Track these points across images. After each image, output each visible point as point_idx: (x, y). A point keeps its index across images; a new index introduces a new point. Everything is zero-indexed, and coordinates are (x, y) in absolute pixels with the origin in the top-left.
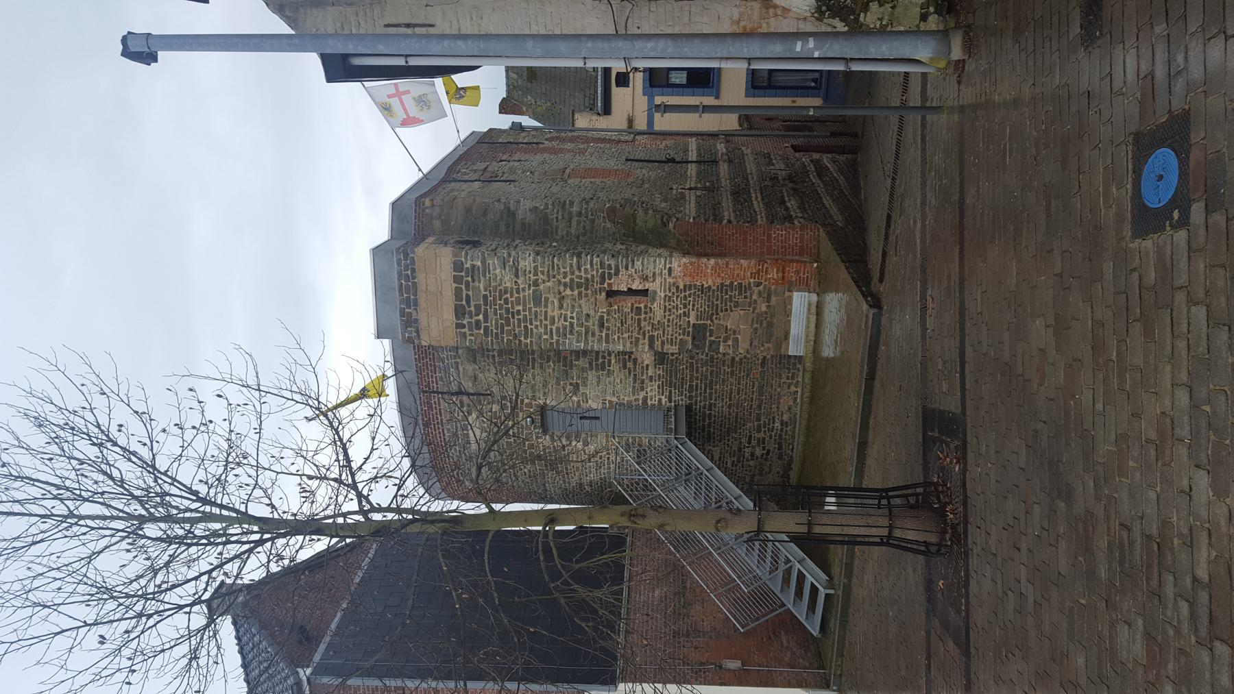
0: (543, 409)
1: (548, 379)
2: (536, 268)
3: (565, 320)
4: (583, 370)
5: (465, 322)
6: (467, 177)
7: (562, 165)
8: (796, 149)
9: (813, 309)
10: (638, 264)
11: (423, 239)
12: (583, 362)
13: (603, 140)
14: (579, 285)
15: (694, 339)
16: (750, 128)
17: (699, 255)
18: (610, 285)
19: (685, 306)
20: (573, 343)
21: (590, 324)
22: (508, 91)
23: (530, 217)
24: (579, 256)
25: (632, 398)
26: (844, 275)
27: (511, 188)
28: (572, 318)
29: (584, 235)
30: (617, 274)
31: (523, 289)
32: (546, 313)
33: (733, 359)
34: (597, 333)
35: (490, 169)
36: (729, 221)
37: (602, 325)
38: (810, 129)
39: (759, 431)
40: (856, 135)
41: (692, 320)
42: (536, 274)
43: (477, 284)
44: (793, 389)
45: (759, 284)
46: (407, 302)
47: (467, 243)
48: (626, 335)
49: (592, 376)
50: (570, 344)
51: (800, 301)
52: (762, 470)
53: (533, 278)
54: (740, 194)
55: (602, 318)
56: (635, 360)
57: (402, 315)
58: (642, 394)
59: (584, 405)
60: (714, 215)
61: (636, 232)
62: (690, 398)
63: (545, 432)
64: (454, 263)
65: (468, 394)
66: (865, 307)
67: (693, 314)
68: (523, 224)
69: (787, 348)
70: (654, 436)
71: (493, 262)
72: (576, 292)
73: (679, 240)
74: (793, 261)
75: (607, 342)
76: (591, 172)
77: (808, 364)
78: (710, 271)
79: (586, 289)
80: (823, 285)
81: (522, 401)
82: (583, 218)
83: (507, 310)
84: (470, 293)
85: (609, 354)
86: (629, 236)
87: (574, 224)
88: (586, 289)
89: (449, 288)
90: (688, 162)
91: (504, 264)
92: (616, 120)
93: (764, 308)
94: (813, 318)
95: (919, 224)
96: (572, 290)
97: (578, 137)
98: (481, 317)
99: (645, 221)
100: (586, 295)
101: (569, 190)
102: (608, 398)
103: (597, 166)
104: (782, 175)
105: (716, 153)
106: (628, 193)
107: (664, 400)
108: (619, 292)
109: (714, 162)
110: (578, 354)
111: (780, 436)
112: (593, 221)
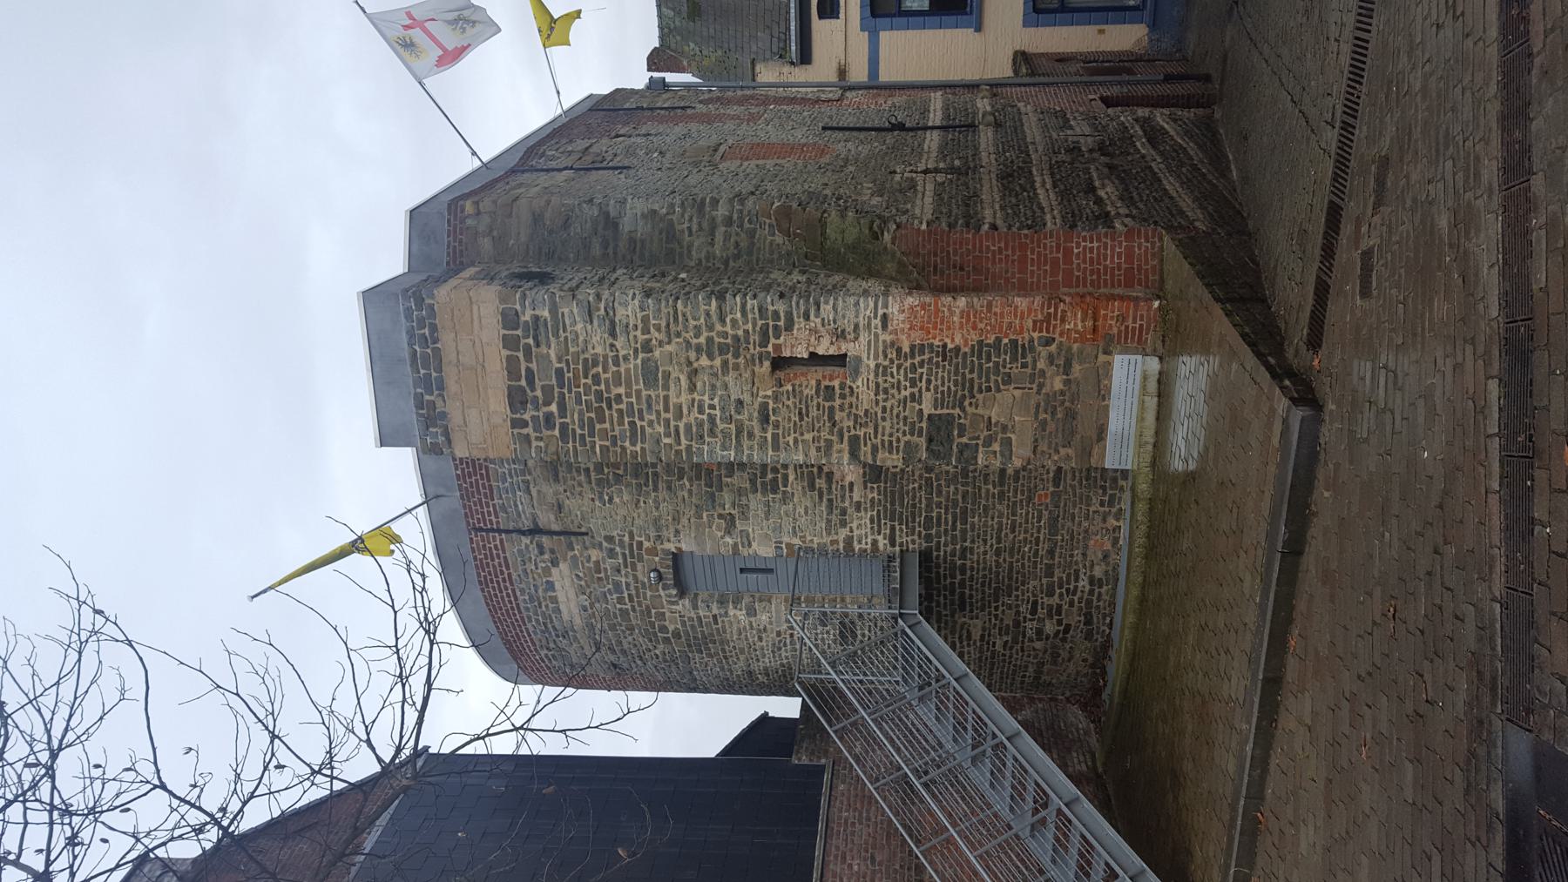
0: (677, 558)
1: (681, 508)
2: (645, 320)
3: (701, 412)
4: (740, 492)
5: (527, 417)
6: (553, 164)
7: (714, 139)
8: (1107, 102)
9: (1152, 386)
10: (827, 309)
11: (457, 272)
12: (739, 480)
13: (792, 100)
14: (723, 350)
15: (930, 440)
16: (1033, 74)
17: (938, 290)
18: (777, 348)
19: (913, 383)
20: (715, 451)
21: (744, 417)
22: (662, 37)
23: (642, 229)
24: (721, 297)
25: (827, 540)
26: (1221, 324)
27: (621, 179)
28: (712, 407)
29: (737, 257)
30: (789, 326)
31: (626, 358)
32: (666, 398)
33: (1003, 471)
34: (757, 432)
35: (594, 149)
36: (994, 227)
37: (765, 419)
38: (1130, 72)
39: (1051, 594)
40: (1207, 78)
41: (927, 408)
42: (646, 331)
43: (544, 349)
44: (1112, 522)
45: (1048, 342)
46: (426, 382)
47: (528, 276)
48: (808, 436)
49: (755, 502)
50: (711, 452)
51: (1128, 372)
52: (1055, 656)
53: (641, 338)
54: (1014, 178)
55: (764, 406)
56: (830, 475)
57: (420, 404)
58: (843, 533)
59: (744, 552)
60: (968, 217)
61: (827, 250)
62: (928, 538)
63: (682, 593)
64: (504, 314)
65: (551, 533)
66: (1282, 403)
67: (928, 398)
68: (632, 241)
69: (1103, 456)
70: (868, 602)
71: (571, 311)
72: (718, 362)
73: (900, 263)
74: (1113, 297)
75: (776, 448)
76: (761, 150)
77: (1143, 487)
78: (959, 319)
79: (736, 356)
80: (1171, 339)
81: (640, 544)
82: (735, 228)
83: (599, 395)
84: (534, 366)
85: (785, 467)
86: (814, 258)
87: (719, 237)
88: (736, 356)
89: (496, 358)
90: (926, 128)
91: (590, 314)
92: (822, 69)
93: (1058, 384)
94: (1152, 403)
95: (1492, 227)
96: (711, 357)
97: (752, 97)
98: (554, 408)
99: (842, 229)
100: (736, 367)
101: (717, 180)
102: (786, 539)
103: (773, 140)
104: (1087, 143)
105: (975, 114)
106: (815, 184)
107: (882, 542)
108: (793, 361)
109: (972, 126)
110: (731, 467)
111: (1089, 602)
112: (751, 234)
